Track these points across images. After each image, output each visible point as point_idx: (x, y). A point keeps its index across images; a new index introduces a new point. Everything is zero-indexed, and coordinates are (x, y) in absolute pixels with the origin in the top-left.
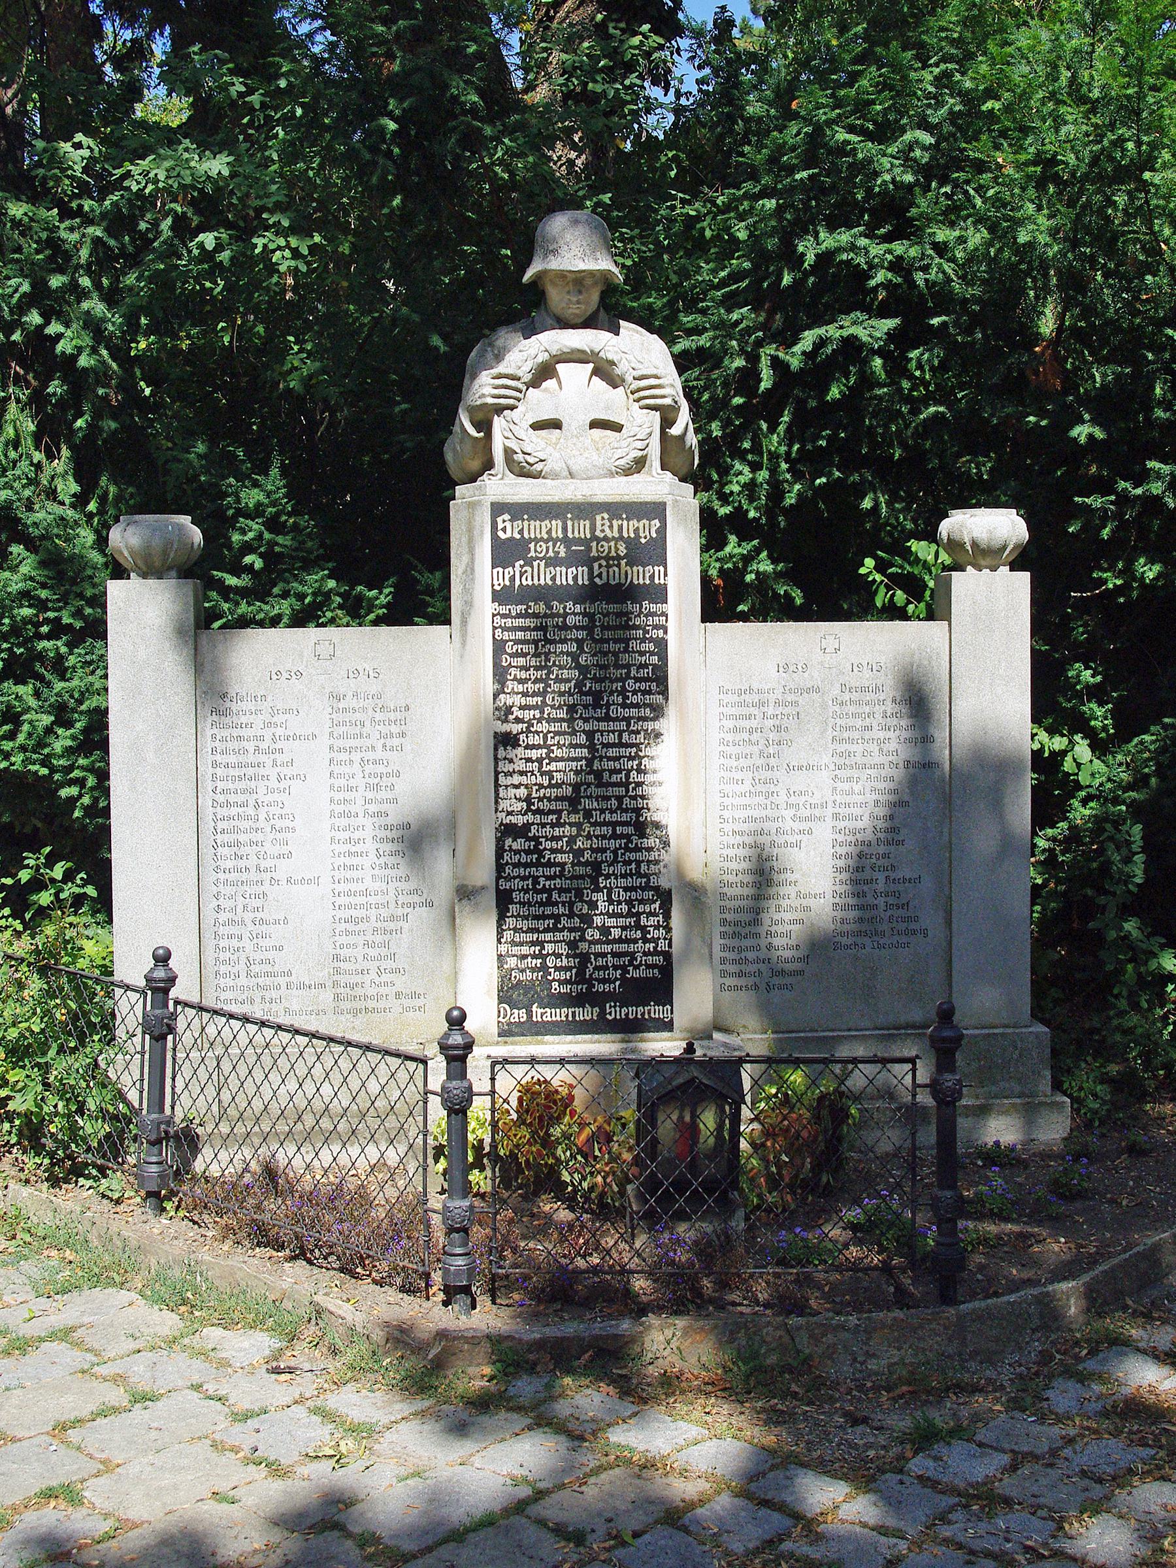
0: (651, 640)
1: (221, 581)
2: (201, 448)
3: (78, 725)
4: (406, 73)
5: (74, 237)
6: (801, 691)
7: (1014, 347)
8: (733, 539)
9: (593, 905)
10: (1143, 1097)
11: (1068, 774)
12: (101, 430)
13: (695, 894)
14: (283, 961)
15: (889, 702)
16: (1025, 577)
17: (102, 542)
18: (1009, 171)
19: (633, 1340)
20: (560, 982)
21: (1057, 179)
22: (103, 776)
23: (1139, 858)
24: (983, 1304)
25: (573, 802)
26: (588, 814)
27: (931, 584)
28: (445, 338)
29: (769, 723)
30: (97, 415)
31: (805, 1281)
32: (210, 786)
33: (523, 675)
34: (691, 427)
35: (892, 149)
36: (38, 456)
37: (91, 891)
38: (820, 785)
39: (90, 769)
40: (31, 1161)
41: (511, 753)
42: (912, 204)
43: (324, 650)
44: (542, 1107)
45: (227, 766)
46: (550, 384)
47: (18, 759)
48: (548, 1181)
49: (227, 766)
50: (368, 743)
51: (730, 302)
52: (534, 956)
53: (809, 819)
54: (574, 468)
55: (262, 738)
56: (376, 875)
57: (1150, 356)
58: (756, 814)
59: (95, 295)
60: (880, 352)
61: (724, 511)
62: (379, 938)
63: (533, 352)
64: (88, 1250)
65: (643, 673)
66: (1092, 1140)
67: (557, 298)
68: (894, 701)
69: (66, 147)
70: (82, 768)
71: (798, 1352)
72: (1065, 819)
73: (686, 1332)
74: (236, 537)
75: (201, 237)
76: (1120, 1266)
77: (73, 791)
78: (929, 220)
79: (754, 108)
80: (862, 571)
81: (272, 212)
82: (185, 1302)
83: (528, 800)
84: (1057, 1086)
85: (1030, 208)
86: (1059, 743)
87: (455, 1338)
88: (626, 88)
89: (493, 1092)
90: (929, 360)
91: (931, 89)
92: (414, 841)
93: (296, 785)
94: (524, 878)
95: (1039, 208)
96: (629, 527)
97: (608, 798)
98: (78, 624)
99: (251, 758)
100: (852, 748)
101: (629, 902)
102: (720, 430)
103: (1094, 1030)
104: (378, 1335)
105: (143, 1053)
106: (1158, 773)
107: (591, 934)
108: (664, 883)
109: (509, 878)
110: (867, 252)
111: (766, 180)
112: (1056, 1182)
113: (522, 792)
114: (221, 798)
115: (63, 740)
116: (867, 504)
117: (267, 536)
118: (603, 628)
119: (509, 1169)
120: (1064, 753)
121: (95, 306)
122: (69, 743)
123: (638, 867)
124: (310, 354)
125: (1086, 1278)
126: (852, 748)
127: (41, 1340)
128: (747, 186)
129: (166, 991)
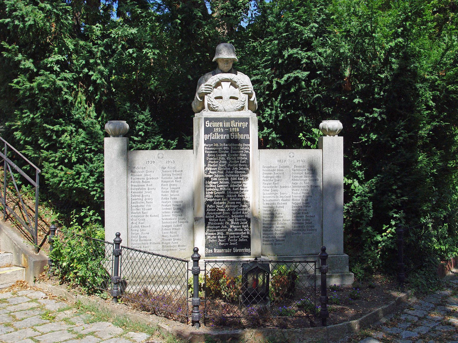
0: (245, 153)
1: (133, 139)
2: (128, 104)
3: (96, 176)
4: (183, 8)
5: (96, 50)
6: (284, 167)
7: (338, 79)
8: (266, 128)
9: (230, 222)
10: (372, 274)
11: (352, 189)
12: (102, 99)
13: (256, 219)
14: (149, 237)
15: (307, 170)
16: (342, 138)
17: (102, 128)
18: (338, 34)
19: (242, 335)
20: (222, 242)
21: (350, 36)
22: (102, 189)
23: (371, 211)
24: (334, 326)
25: (225, 195)
26: (229, 198)
27: (317, 140)
28: (191, 76)
29: (276, 175)
30: (101, 95)
31: (286, 320)
32: (130, 191)
33: (212, 162)
34: (256, 99)
35: (307, 28)
36: (86, 106)
37: (99, 218)
38: (289, 192)
39: (99, 187)
40: (83, 289)
41: (209, 183)
42: (313, 42)
43: (160, 156)
44: (216, 275)
45: (135, 186)
46: (220, 87)
47: (80, 184)
48: (218, 294)
49: (135, 186)
50: (172, 180)
51: (266, 67)
52: (215, 236)
53: (286, 200)
54: (226, 109)
55: (144, 179)
56: (172, 215)
57: (374, 81)
58: (272, 199)
59: (101, 65)
60: (304, 80)
61: (263, 121)
62: (174, 231)
63: (215, 79)
64: (98, 312)
65: (243, 162)
66: (360, 285)
67: (221, 65)
68: (308, 170)
69: (94, 27)
70: (97, 187)
71: (285, 338)
72: (352, 201)
73: (256, 333)
74: (137, 127)
75: (129, 50)
76: (368, 316)
77: (94, 193)
78: (317, 46)
79: (270, 19)
80: (299, 136)
81: (148, 43)
82: (124, 325)
83: (213, 195)
84: (350, 270)
85: (343, 43)
86: (350, 181)
87: (195, 334)
88: (238, 13)
89: (205, 270)
90: (317, 83)
91: (317, 13)
92: (181, 209)
93: (153, 191)
94: (212, 215)
95: (346, 43)
96: (240, 124)
97: (234, 194)
98: (96, 150)
99: (141, 184)
100: (297, 182)
101: (239, 222)
102: (264, 99)
103: (359, 256)
104: (175, 334)
105: (113, 260)
106: (376, 189)
107: (229, 230)
108: (248, 216)
109: (208, 215)
110: (301, 55)
111: (275, 36)
112: (351, 295)
113: (212, 193)
114: (133, 194)
115: (92, 179)
116: (300, 119)
117: (145, 127)
118: (233, 150)
119: (208, 291)
120: (351, 184)
121: (101, 67)
122: (93, 180)
123: (242, 212)
124: (156, 80)
125: (360, 319)
126: (297, 182)
127: (86, 335)
128: (270, 37)
129: (119, 244)
